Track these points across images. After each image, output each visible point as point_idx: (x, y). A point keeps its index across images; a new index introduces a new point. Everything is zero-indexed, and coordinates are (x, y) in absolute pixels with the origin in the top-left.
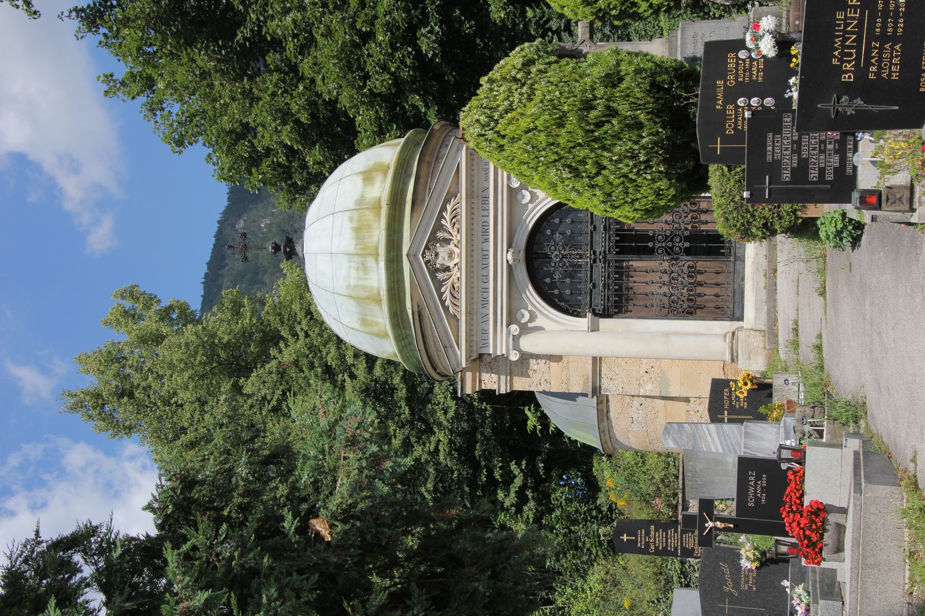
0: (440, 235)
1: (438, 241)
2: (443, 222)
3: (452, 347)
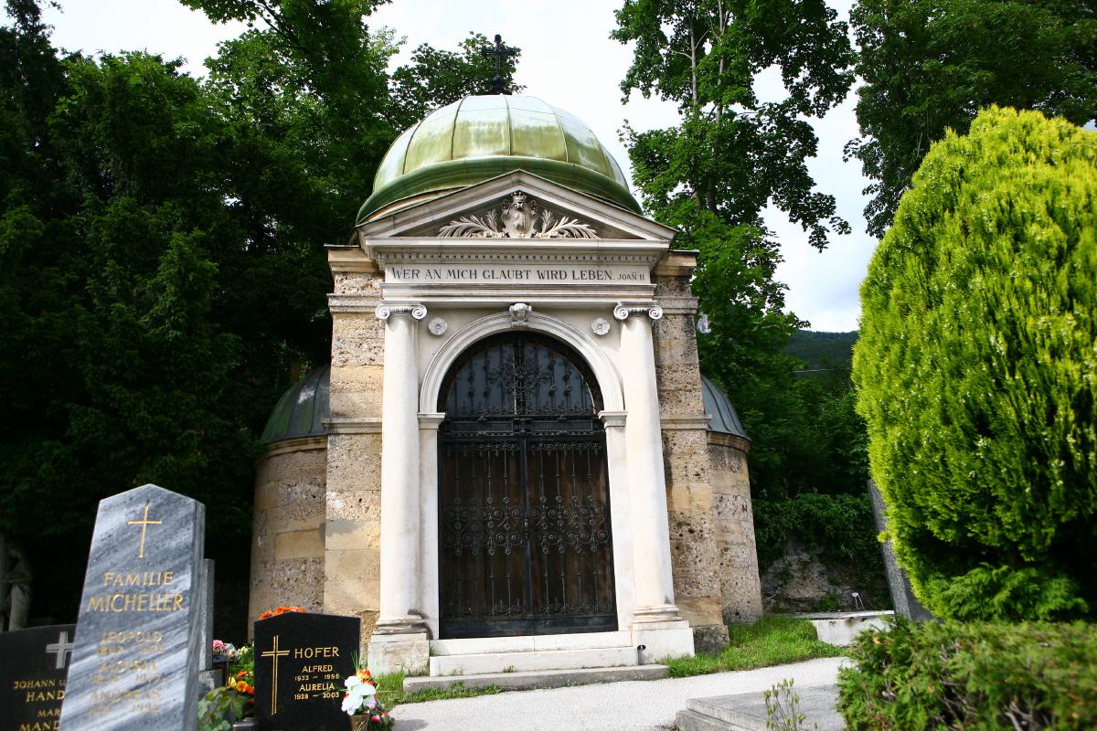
0: (547, 215)
1: (540, 212)
2: (564, 220)
3: (395, 226)
